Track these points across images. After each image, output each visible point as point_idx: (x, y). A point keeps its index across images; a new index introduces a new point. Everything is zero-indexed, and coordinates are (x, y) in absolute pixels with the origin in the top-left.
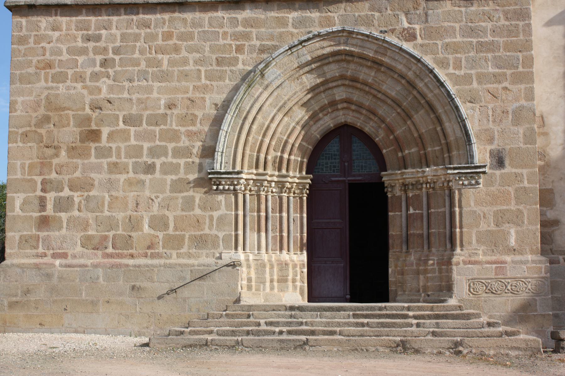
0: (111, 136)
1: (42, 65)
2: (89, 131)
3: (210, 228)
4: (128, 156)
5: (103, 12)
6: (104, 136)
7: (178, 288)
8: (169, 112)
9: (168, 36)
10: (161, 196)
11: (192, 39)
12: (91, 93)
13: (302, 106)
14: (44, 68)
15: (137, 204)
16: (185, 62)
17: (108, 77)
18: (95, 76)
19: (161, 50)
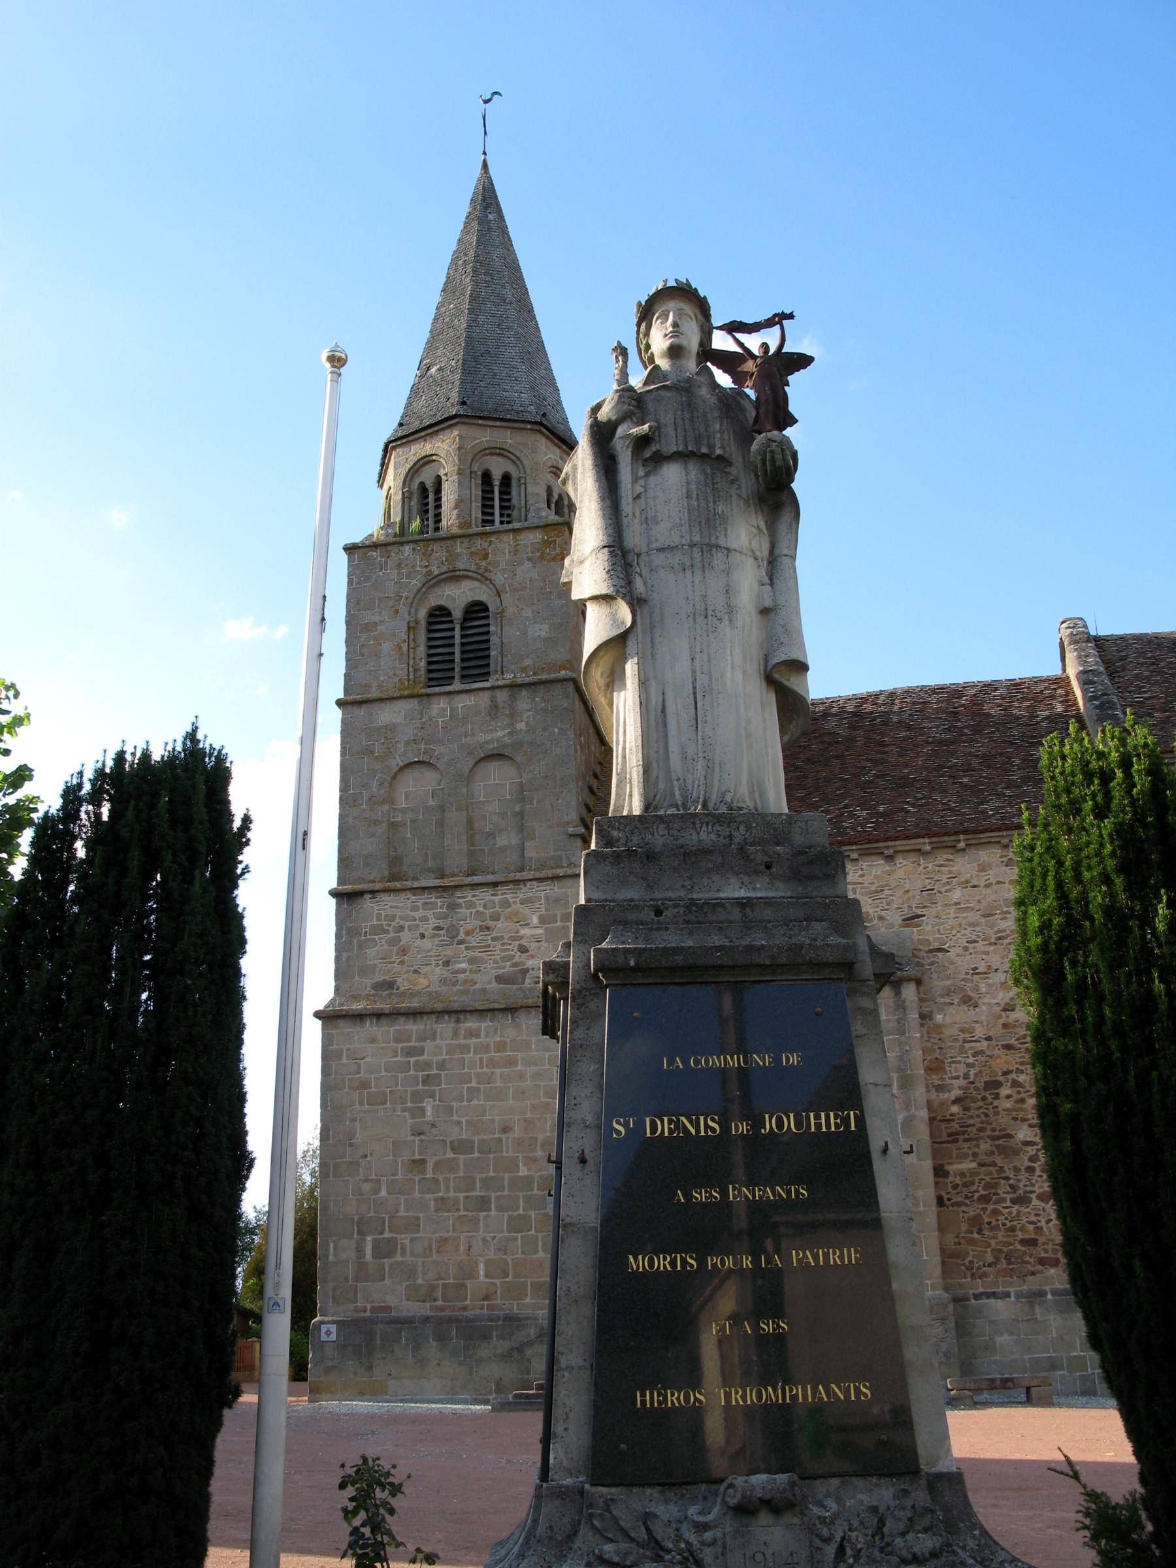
0: (437, 1165)
1: (356, 1084)
2: (413, 1160)
3: (507, 1152)
4: (458, 1189)
5: (610, 521)
6: (430, 1165)
7: (381, 700)
8: (504, 1136)
9: (501, 1046)
10: (498, 1236)
11: (529, 1048)
12: (413, 1116)
13: (1050, 1385)
14: (358, 1088)
15: (470, 1247)
16: (521, 1076)
17: (433, 1096)
18: (417, 1097)
19: (492, 1063)
